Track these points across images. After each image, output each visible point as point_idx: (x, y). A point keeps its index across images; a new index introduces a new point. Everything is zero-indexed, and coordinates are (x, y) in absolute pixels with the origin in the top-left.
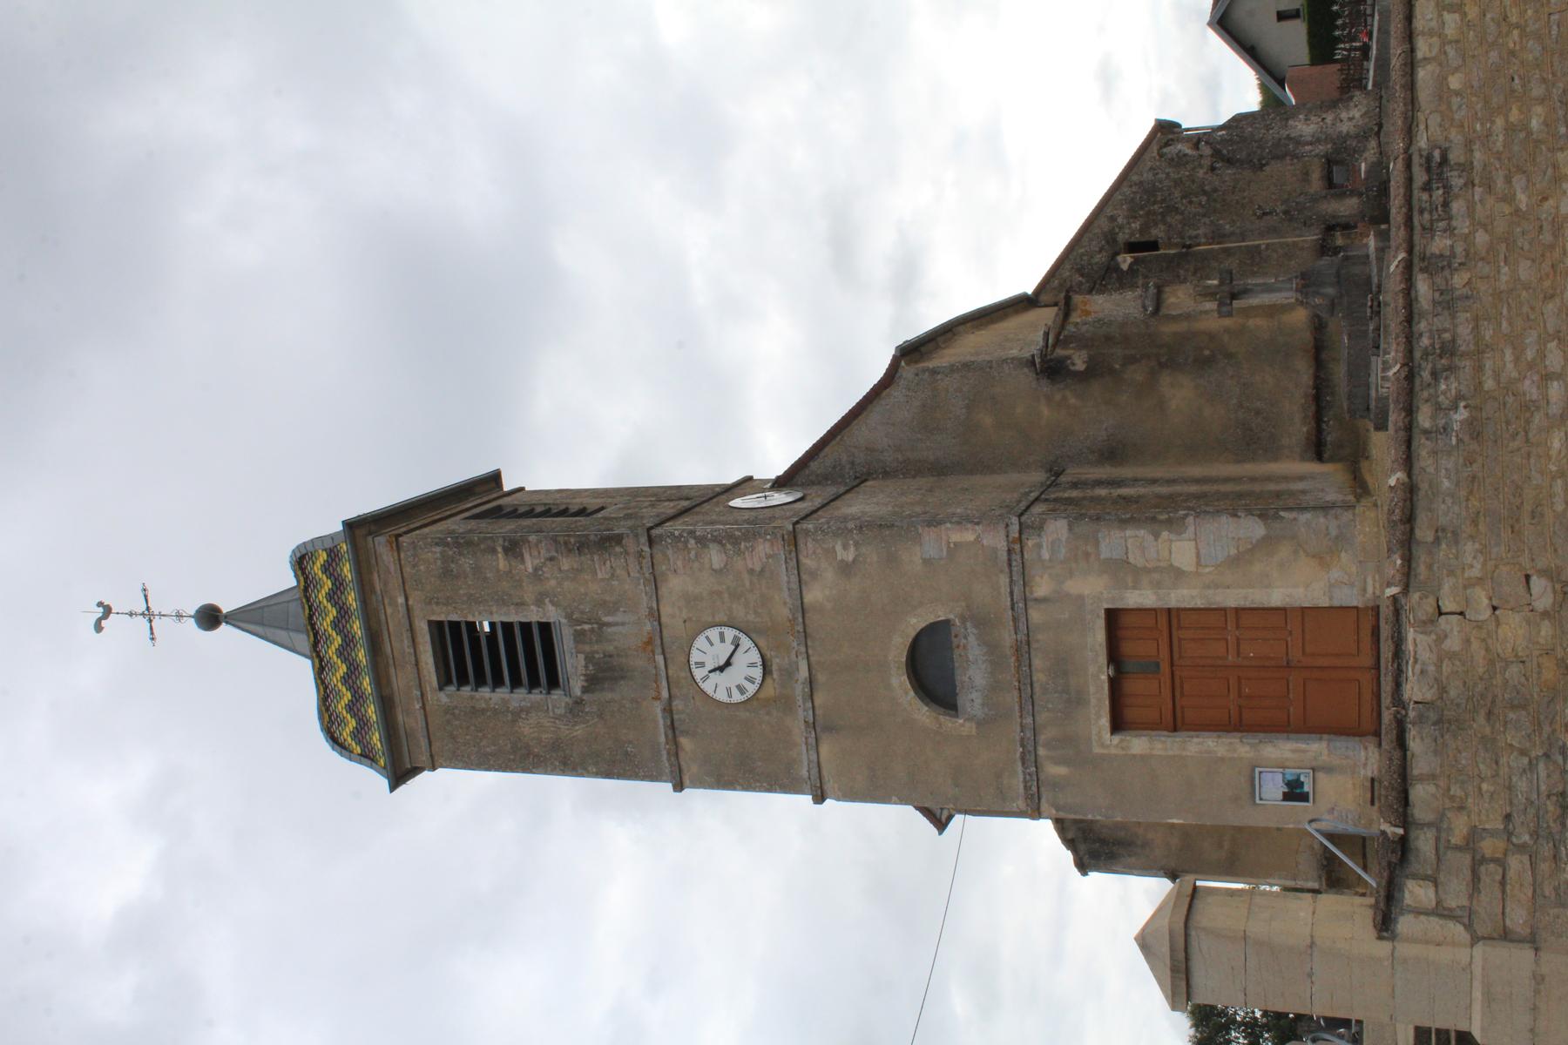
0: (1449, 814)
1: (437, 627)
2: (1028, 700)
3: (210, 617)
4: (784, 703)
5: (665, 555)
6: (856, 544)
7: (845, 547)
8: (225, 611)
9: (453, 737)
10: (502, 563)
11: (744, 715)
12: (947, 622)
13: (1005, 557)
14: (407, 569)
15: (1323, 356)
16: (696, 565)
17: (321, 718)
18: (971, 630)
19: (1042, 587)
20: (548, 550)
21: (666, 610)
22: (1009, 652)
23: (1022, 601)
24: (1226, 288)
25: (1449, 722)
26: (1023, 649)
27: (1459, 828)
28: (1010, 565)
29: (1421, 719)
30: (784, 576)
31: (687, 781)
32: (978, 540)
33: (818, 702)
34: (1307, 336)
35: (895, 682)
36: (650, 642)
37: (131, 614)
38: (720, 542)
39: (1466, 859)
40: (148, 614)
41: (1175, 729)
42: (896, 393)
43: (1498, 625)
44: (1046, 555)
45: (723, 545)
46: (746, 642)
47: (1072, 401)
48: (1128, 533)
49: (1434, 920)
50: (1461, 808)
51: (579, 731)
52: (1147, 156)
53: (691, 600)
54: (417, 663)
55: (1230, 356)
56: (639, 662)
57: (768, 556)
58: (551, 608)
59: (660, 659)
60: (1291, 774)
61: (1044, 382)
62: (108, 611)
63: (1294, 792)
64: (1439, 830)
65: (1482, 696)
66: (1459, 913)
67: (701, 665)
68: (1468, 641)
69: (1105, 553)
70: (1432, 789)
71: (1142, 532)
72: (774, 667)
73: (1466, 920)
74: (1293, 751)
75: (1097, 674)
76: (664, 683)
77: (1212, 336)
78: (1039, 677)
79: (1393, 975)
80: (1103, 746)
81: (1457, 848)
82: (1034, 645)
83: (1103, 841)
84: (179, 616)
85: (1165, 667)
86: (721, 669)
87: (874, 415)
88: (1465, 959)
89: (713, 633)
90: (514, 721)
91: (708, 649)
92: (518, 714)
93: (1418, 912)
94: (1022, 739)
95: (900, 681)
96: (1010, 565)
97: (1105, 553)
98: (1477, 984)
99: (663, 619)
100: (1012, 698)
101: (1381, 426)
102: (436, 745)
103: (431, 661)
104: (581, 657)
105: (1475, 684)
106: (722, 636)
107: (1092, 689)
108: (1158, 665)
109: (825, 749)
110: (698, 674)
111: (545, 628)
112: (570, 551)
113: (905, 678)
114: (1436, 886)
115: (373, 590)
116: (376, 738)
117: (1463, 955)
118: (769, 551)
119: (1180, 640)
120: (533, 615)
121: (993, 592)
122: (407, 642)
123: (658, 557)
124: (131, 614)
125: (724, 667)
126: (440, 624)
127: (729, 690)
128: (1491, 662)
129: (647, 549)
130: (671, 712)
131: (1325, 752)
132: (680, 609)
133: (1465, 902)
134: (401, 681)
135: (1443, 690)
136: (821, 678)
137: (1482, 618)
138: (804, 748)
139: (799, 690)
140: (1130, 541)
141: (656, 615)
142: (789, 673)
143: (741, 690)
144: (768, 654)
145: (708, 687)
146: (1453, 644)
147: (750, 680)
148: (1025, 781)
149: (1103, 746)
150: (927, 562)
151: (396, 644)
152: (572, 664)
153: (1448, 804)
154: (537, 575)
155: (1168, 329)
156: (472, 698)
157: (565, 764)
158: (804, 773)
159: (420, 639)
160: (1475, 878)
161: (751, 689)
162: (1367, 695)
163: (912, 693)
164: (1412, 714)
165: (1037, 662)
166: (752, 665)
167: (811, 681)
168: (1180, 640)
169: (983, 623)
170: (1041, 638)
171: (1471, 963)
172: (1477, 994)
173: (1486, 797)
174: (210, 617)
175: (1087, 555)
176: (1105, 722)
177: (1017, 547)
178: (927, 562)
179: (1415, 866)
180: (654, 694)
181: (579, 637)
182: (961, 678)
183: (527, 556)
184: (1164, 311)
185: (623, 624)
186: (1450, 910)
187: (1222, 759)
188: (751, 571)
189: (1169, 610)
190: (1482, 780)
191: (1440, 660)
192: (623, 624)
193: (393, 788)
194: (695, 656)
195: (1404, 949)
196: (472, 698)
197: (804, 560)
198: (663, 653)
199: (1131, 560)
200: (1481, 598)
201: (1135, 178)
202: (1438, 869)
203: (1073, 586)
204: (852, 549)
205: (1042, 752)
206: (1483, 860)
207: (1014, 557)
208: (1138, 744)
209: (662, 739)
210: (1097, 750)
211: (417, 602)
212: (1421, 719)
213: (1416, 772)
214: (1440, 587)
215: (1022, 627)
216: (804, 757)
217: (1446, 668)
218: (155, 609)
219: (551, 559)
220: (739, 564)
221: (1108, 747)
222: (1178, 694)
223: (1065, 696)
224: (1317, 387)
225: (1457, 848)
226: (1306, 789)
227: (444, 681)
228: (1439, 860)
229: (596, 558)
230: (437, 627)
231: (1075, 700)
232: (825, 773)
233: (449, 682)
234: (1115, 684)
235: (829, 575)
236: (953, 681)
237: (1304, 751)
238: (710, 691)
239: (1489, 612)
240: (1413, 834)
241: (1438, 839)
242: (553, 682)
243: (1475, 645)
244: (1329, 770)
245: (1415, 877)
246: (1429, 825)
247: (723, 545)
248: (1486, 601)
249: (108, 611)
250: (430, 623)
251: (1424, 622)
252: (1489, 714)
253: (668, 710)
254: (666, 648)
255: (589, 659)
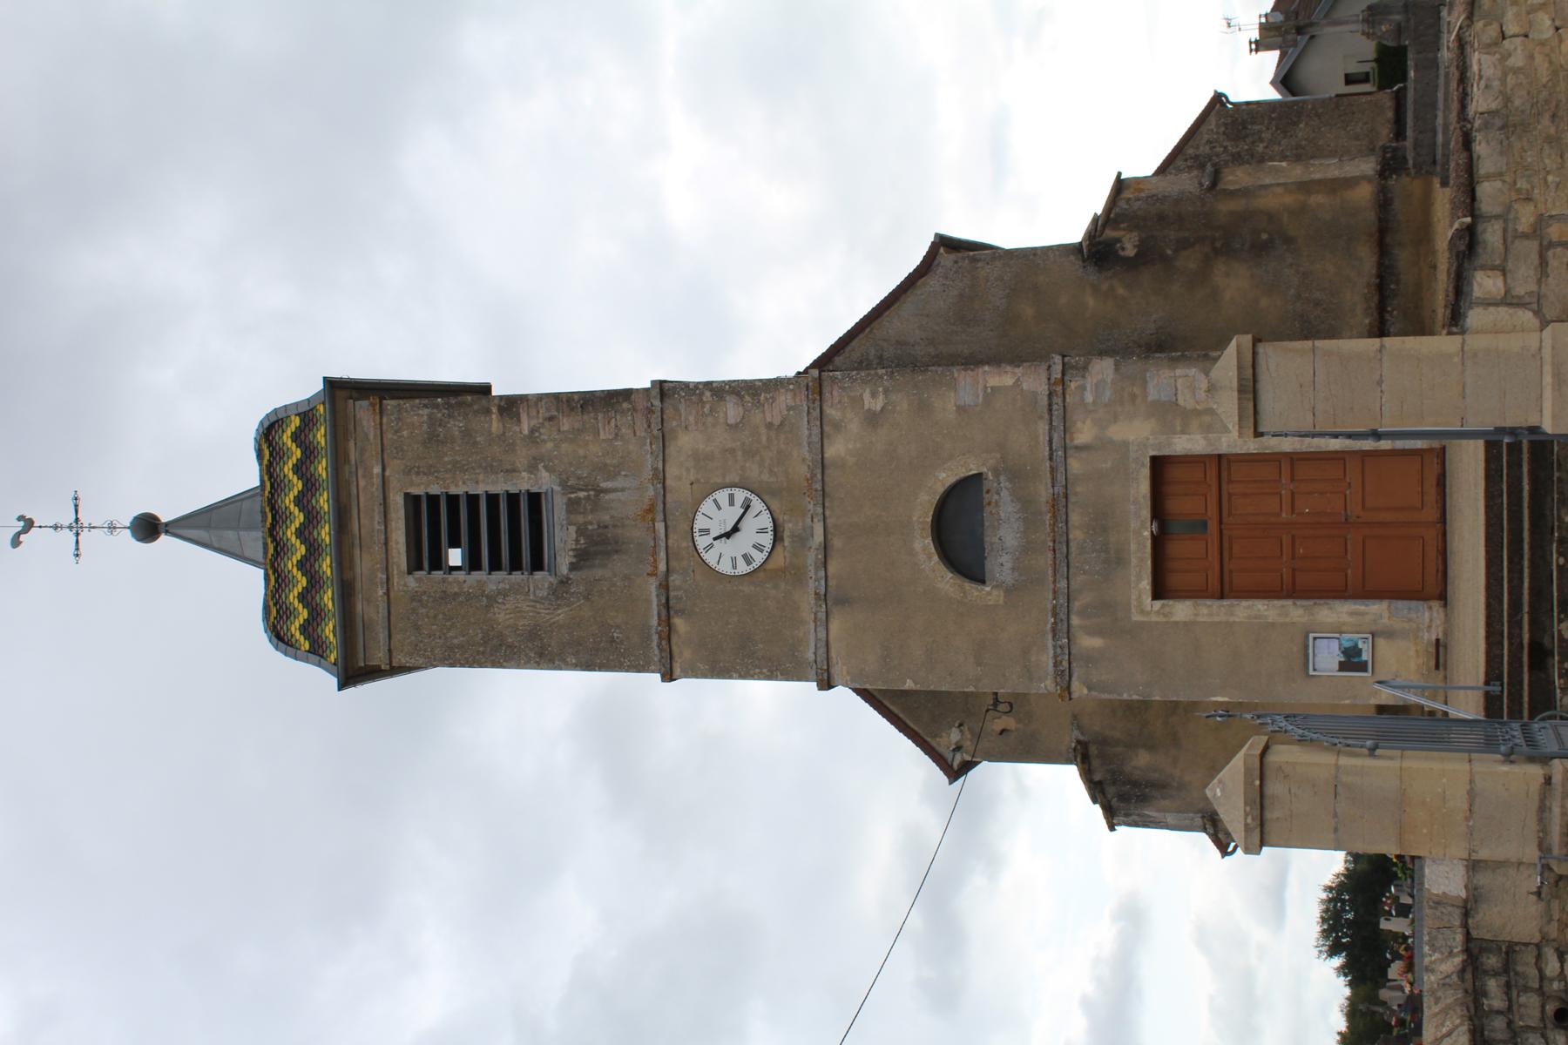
0: (1516, 206)
1: (413, 501)
2: (1063, 560)
3: (148, 528)
4: (794, 574)
5: (677, 410)
6: (886, 392)
7: (874, 395)
8: (164, 520)
9: (417, 628)
10: (495, 425)
11: (747, 589)
12: (978, 478)
13: (1045, 401)
14: (389, 436)
15: (1388, 239)
16: (710, 420)
17: (266, 609)
18: (1005, 483)
19: (1084, 433)
20: (548, 410)
21: (672, 471)
22: (1044, 508)
23: (1061, 449)
24: (1292, 23)
25: (1515, 126)
26: (1060, 504)
27: (1525, 217)
28: (1050, 410)
29: (1486, 126)
30: (805, 430)
31: (677, 671)
32: (1017, 384)
33: (832, 569)
34: (1371, 216)
35: (918, 545)
36: (651, 509)
37: (56, 527)
38: (738, 394)
39: (1532, 246)
40: (77, 527)
41: (1222, 597)
42: (933, 282)
43: (1561, 41)
44: (1089, 398)
45: (742, 398)
46: (757, 505)
47: (1121, 291)
48: (1179, 372)
49: (1503, 310)
50: (1528, 199)
51: (561, 615)
52: (1204, 129)
53: (698, 458)
54: (386, 543)
55: (1289, 241)
56: (637, 533)
57: (789, 409)
58: (544, 474)
59: (660, 526)
60: (1347, 639)
61: (1091, 269)
62: (29, 524)
63: (1351, 661)
64: (1506, 221)
65: (1547, 102)
66: (1527, 299)
67: (706, 532)
68: (1532, 57)
69: (1153, 395)
70: (1498, 184)
71: (1193, 371)
72: (786, 534)
73: (1535, 306)
74: (1352, 614)
75: (1139, 531)
76: (663, 555)
77: (1271, 217)
78: (1076, 535)
79: (1463, 372)
80: (1142, 612)
81: (1525, 236)
82: (1072, 499)
83: (1135, 784)
84: (112, 528)
85: (1213, 526)
86: (728, 535)
87: (908, 306)
88: (1535, 345)
89: (722, 496)
90: (489, 607)
91: (715, 514)
92: (492, 599)
93: (1488, 303)
94: (1055, 607)
95: (924, 544)
96: (1050, 410)
97: (1153, 395)
98: (1547, 369)
99: (668, 482)
100: (1044, 561)
101: (1444, 184)
102: (397, 637)
103: (403, 548)
104: (573, 529)
105: (1539, 92)
106: (731, 497)
107: (1133, 547)
108: (1205, 524)
109: (835, 626)
110: (702, 542)
111: (535, 499)
112: (572, 409)
113: (929, 541)
114: (1504, 275)
115: (347, 460)
116: (329, 630)
117: (1532, 340)
118: (790, 402)
119: (1230, 495)
120: (523, 484)
121: (1029, 440)
122: (378, 518)
123: (669, 412)
124: (56, 527)
125: (731, 534)
126: (417, 498)
127: (734, 560)
128: (1555, 73)
129: (657, 403)
130: (667, 588)
131: (1386, 614)
132: (688, 470)
133: (1534, 288)
134: (365, 564)
135: (1507, 100)
136: (837, 543)
137: (1545, 36)
138: (812, 625)
139: (812, 557)
140: (1180, 381)
141: (660, 477)
142: (802, 540)
143: (748, 559)
144: (781, 518)
145: (711, 558)
146: (1517, 60)
147: (758, 547)
148: (1055, 656)
149: (1142, 612)
150: (961, 409)
151: (366, 521)
152: (562, 539)
153: (1514, 196)
154: (533, 437)
155: (1225, 207)
156: (444, 581)
157: (541, 655)
158: (811, 657)
159: (392, 515)
160: (1543, 262)
161: (759, 558)
162: (1432, 553)
163: (936, 558)
164: (1477, 124)
165: (1075, 518)
166: (762, 531)
167: (826, 547)
168: (1230, 495)
169: (1017, 475)
170: (1080, 490)
171: (1540, 349)
172: (1548, 379)
173: (1552, 187)
174: (148, 528)
175: (1133, 397)
176: (1146, 585)
177: (1059, 389)
178: (961, 409)
179: (1483, 257)
180: (650, 569)
181: (573, 506)
182: (990, 539)
183: (524, 417)
184: (1221, 186)
185: (623, 490)
186: (1519, 297)
187: (1273, 624)
188: (769, 426)
189: (1220, 456)
190: (1548, 173)
191: (1505, 74)
192: (623, 490)
193: (341, 687)
194: (700, 522)
195: (1474, 342)
196: (444, 581)
197: (828, 411)
198: (665, 520)
199: (1181, 402)
200: (1544, 21)
201: (1191, 151)
202: (1505, 260)
203: (1118, 432)
204: (881, 397)
205: (1075, 621)
206: (1551, 245)
207: (1055, 400)
208: (1182, 610)
209: (654, 621)
210: (1137, 617)
211: (389, 482)
212: (1486, 126)
213: (1482, 172)
214: (1503, 15)
215: (1061, 478)
216: (812, 637)
217: (1511, 80)
218: (84, 520)
219: (551, 419)
220: (757, 418)
221: (1148, 613)
222: (1226, 554)
223: (1103, 555)
224: (1380, 276)
225: (1525, 236)
226: (1366, 656)
227: (415, 565)
228: (1506, 249)
229: (600, 416)
230: (413, 501)
231: (1116, 560)
232: (833, 654)
233: (420, 568)
234: (1158, 543)
235: (854, 426)
236: (982, 541)
237: (1363, 614)
238: (713, 563)
239: (1551, 32)
240: (1480, 228)
241: (1505, 230)
242: (537, 565)
243: (1539, 59)
244: (1390, 634)
245: (1483, 268)
246: (1497, 217)
247: (742, 398)
248: (1548, 23)
249: (29, 524)
250: (407, 495)
251: (1489, 45)
252: (1554, 116)
253: (665, 587)
254: (670, 513)
255: (581, 531)
